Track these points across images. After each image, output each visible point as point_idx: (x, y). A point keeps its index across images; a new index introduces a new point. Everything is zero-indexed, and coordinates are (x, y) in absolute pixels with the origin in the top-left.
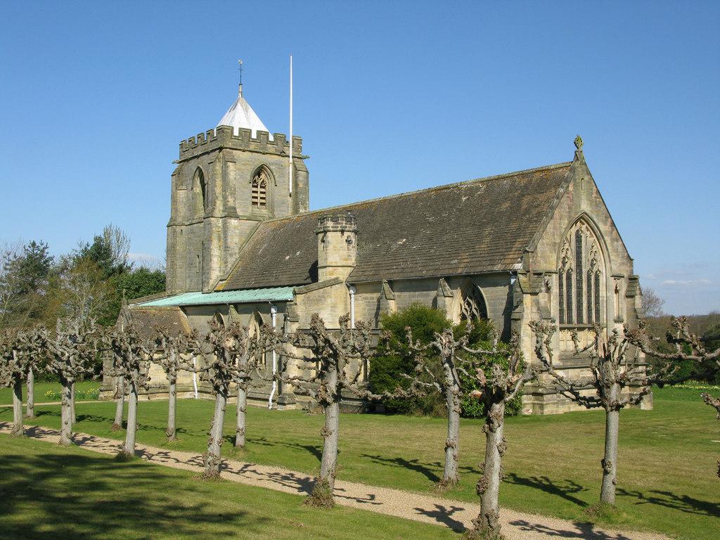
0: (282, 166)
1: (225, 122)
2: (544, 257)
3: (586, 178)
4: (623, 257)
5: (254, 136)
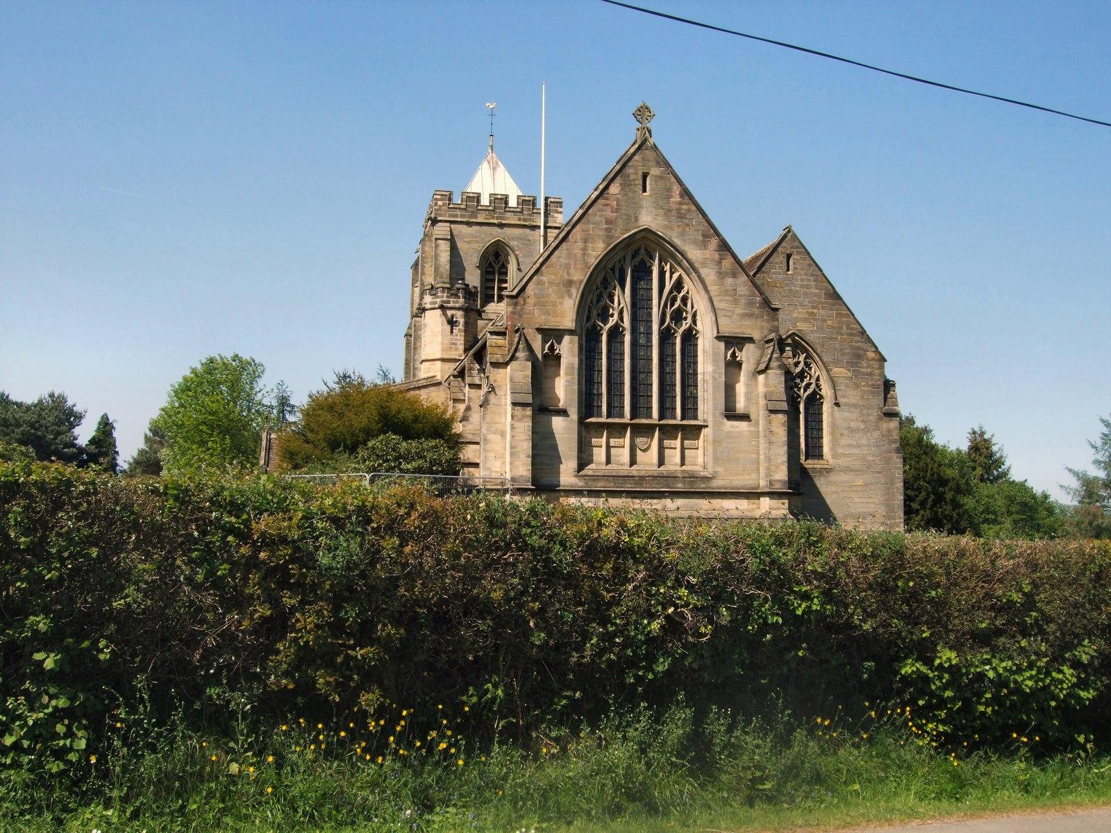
0: (529, 240)
1: (474, 188)
2: (540, 304)
3: (655, 171)
4: (750, 304)
5: (485, 201)
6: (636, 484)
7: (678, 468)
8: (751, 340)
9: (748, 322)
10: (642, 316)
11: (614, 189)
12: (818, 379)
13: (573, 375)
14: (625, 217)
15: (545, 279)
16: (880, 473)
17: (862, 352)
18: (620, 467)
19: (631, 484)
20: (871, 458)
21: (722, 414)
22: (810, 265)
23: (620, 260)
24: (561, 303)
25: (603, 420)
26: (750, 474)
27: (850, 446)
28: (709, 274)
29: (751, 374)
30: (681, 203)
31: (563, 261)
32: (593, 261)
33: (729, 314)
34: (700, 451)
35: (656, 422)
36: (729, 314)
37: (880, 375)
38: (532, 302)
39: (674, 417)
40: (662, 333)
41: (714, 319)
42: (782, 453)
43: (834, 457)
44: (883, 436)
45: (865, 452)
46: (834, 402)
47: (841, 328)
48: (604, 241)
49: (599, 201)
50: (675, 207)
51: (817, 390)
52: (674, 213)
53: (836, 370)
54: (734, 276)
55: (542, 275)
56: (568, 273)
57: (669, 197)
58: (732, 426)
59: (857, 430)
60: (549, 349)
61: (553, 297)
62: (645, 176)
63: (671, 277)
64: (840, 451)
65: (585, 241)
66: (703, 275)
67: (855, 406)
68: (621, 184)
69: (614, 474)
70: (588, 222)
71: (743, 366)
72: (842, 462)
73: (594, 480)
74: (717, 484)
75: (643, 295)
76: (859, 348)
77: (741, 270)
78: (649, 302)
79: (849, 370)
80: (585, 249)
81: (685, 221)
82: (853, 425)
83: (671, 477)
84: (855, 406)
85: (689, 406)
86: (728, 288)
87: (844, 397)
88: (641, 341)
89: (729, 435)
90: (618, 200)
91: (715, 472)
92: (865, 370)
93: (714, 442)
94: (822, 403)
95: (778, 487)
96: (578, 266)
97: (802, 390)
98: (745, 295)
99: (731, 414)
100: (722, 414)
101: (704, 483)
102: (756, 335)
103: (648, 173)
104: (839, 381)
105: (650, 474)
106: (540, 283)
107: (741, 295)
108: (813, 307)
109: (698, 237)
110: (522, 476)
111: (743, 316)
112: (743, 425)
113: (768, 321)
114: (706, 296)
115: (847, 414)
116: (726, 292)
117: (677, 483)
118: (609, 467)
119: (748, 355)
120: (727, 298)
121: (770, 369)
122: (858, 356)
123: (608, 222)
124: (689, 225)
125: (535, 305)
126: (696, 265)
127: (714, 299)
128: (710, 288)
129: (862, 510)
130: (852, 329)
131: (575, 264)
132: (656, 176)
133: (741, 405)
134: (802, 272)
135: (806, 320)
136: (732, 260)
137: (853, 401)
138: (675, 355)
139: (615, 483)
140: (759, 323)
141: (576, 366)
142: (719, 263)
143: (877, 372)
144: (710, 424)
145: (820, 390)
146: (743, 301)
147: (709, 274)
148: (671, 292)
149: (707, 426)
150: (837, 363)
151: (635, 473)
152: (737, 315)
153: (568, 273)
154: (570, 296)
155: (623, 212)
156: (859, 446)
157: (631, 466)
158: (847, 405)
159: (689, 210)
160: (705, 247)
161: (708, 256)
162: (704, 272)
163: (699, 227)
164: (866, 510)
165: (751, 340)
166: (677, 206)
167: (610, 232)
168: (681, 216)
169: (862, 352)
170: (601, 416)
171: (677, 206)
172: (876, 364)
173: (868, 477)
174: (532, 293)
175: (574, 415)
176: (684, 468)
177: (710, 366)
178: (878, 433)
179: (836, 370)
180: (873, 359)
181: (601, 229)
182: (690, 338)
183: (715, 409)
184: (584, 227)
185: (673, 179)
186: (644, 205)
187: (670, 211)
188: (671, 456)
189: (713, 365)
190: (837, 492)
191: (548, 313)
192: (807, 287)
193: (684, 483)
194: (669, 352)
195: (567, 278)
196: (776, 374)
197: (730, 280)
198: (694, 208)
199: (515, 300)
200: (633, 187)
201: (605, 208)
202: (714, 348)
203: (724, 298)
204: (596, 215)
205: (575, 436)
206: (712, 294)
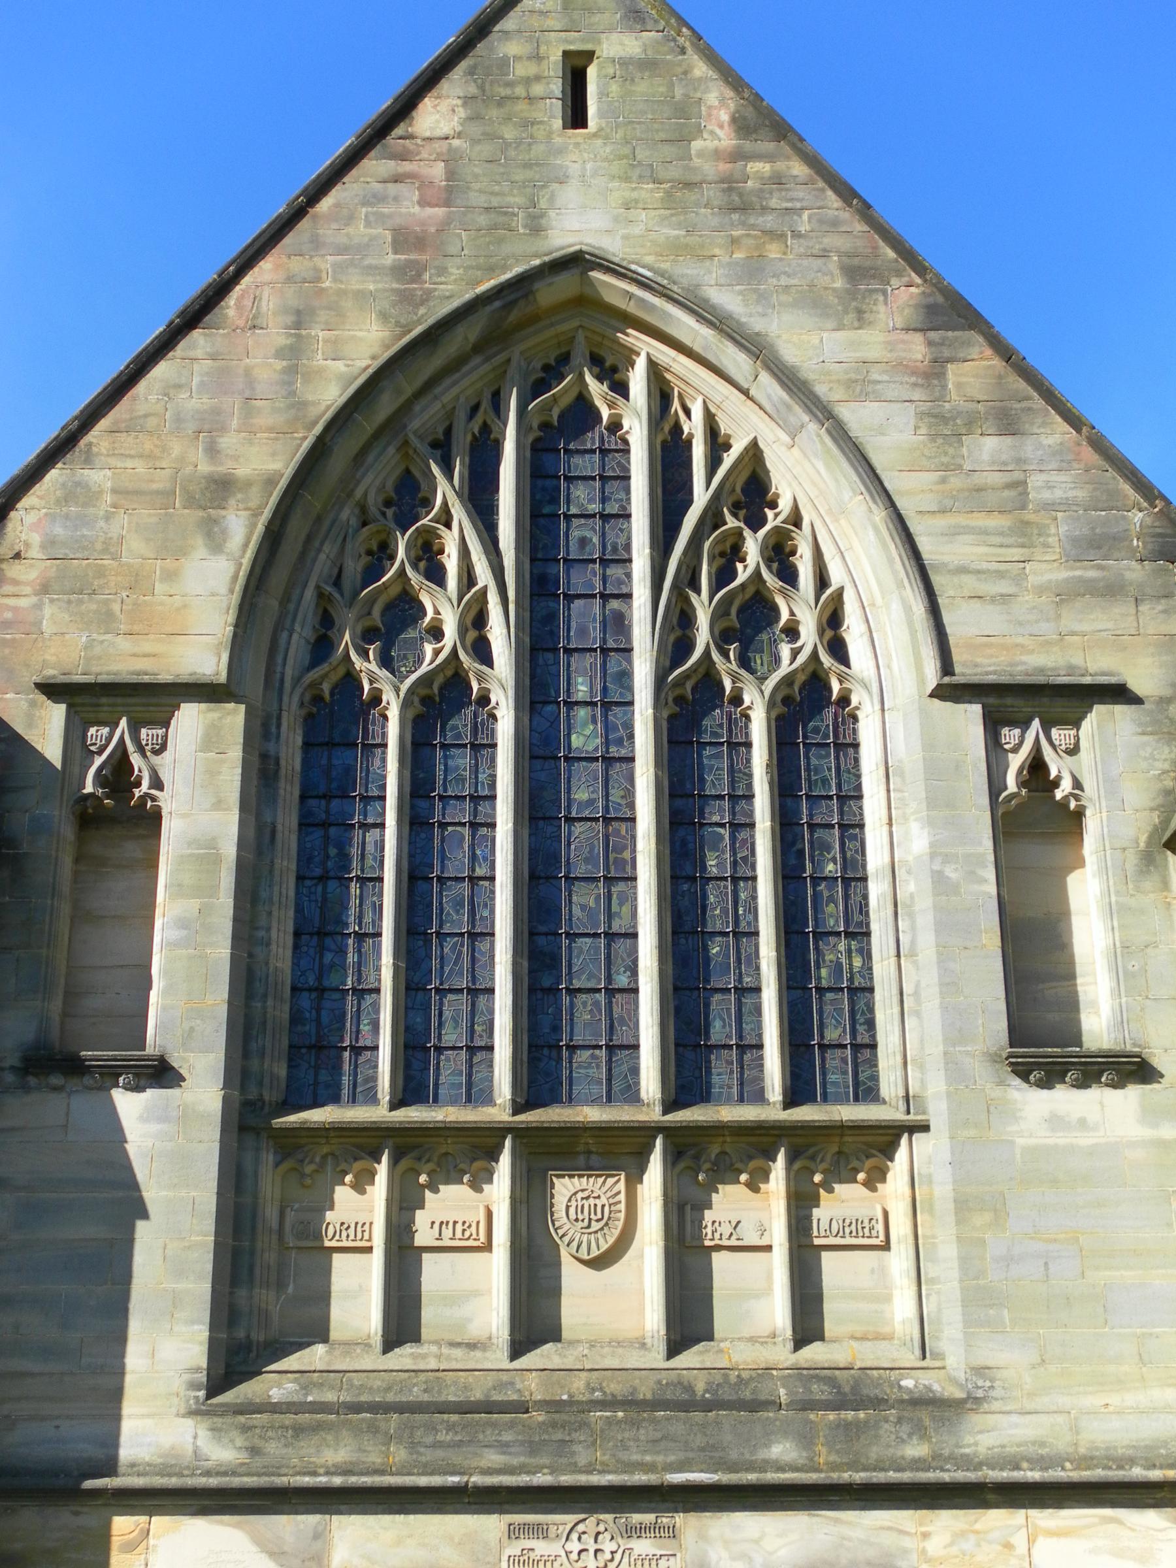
6: (533, 1448)
7: (782, 1354)
8: (1118, 693)
10: (583, 632)
13: (213, 891)
14: (483, 220)
15: (98, 477)
18: (459, 1358)
19: (503, 1447)
21: (994, 1058)
23: (475, 409)
24: (171, 576)
25: (379, 1113)
29: (1132, 860)
30: (737, 156)
31: (193, 403)
33: (1004, 587)
34: (899, 1261)
35: (654, 1114)
36: (1004, 587)
38: (33, 575)
39: (753, 1093)
40: (680, 700)
41: (919, 608)
46: (932, 677)
48: (384, 316)
49: (365, 163)
50: (711, 169)
52: (712, 193)
55: (88, 461)
56: (212, 451)
57: (682, 139)
58: (1056, 1121)
60: (99, 779)
61: (136, 548)
63: (713, 463)
65: (300, 319)
66: (855, 429)
68: (467, 100)
69: (416, 1394)
70: (317, 243)
71: (1092, 824)
73: (299, 1431)
75: (583, 542)
77: (1039, 402)
78: (614, 571)
85: (831, 1035)
86: (978, 479)
88: (576, 741)
90: (451, 160)
91: (980, 1371)
93: (963, 1206)
96: (262, 421)
98: (1066, 505)
100: (994, 1058)
101: (920, 1431)
103: (589, 56)
105: (615, 1387)
106: (73, 494)
107: (1049, 507)
109: (824, 281)
111: (1066, 594)
114: (880, 515)
117: (768, 1439)
118: (403, 1357)
120: (981, 521)
123: (404, 239)
124: (775, 236)
125: (44, 589)
126: (821, 390)
131: (248, 412)
132: (624, 62)
136: (997, 363)
138: (750, 797)
139: (413, 1446)
141: (229, 850)
144: (937, 1112)
146: (1061, 529)
148: (711, 518)
149: (925, 1128)
151: (533, 1388)
152: (1040, 590)
153: (212, 451)
154: (216, 545)
155: (477, 199)
157: (674, 1348)
159: (778, 180)
160: (862, 319)
161: (874, 353)
163: (830, 241)
165: (1118, 693)
166: (724, 167)
167: (417, 278)
170: (373, 1100)
171: (724, 167)
174: (36, 539)
176: (813, 1353)
177: (915, 827)
181: (372, 270)
183: (956, 1035)
184: (297, 265)
185: (701, 69)
186: (574, 169)
187: (688, 185)
188: (452, 1299)
189: (930, 822)
191: (106, 620)
193: (806, 1439)
194: (717, 782)
195: (204, 468)
198: (799, 169)
200: (522, 106)
201: (392, 188)
202: (929, 745)
203: (962, 520)
204: (351, 218)
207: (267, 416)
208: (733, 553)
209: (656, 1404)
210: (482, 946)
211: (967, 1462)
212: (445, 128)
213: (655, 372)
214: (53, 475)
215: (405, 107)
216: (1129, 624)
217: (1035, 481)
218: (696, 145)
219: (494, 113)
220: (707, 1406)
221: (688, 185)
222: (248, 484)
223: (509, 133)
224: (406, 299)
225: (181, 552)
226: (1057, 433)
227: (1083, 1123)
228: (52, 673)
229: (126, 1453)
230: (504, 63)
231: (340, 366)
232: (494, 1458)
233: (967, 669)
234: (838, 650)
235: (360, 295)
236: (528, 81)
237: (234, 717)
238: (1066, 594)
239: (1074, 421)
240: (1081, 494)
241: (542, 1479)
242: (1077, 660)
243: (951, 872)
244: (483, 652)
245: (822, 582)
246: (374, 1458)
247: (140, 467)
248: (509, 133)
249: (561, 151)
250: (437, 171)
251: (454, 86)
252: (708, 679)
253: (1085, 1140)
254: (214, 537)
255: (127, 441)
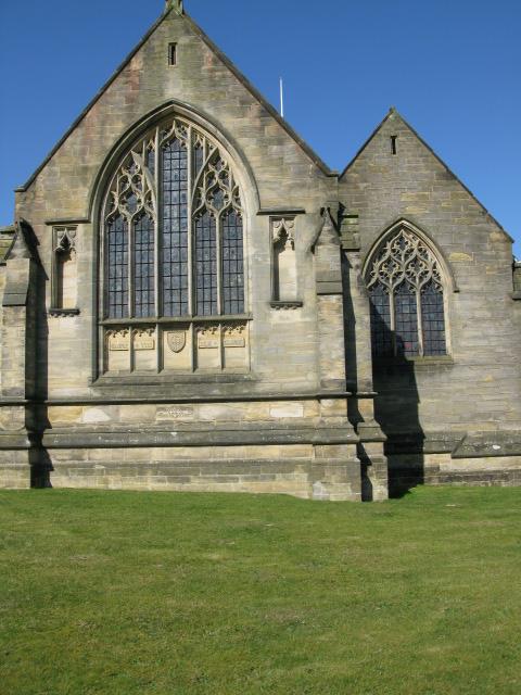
2: (52, 196)
4: (301, 173)
9: (297, 194)
11: (136, 64)
12: (435, 267)
13: (87, 270)
15: (57, 169)
16: (513, 366)
17: (484, 233)
20: (501, 350)
22: (418, 146)
26: (306, 375)
27: (475, 337)
28: (249, 145)
30: (212, 71)
32: (110, 143)
34: (246, 350)
37: (506, 257)
42: (337, 346)
43: (455, 351)
44: (515, 324)
45: (493, 344)
47: (458, 210)
48: (123, 121)
51: (435, 278)
53: (454, 255)
54: (280, 142)
55: (54, 165)
56: (83, 161)
58: (281, 318)
59: (483, 320)
62: (173, 46)
63: (207, 154)
64: (463, 343)
67: (479, 293)
68: (144, 59)
72: (467, 356)
74: (262, 388)
76: (480, 230)
79: (470, 255)
80: (102, 132)
81: (221, 89)
82: (478, 314)
83: (207, 381)
84: (479, 293)
87: (465, 283)
89: (278, 329)
92: (489, 253)
94: (441, 292)
95: (332, 389)
97: (417, 280)
99: (277, 302)
102: (310, 208)
104: (459, 266)
105: (180, 380)
106: (52, 174)
108: (424, 190)
110: (14, 389)
112: (294, 316)
113: (324, 190)
115: (469, 303)
116: (271, 162)
119: (301, 231)
121: (321, 244)
122: (480, 238)
124: (222, 92)
127: (255, 171)
128: (250, 158)
129: (491, 409)
130: (471, 209)
133: (288, 291)
134: (410, 154)
135: (416, 203)
137: (476, 287)
140: (313, 193)
141: (91, 260)
142: (262, 128)
143: (503, 254)
145: (439, 278)
147: (249, 145)
148: (206, 168)
150: (455, 246)
151: (162, 380)
153: (83, 161)
156: (485, 337)
158: (470, 292)
159: (224, 77)
162: (242, 141)
164: (497, 408)
165: (303, 212)
168: (214, 84)
169: (484, 233)
170: (127, 317)
172: (502, 246)
173: (498, 372)
175: (87, 315)
178: (508, 321)
179: (454, 255)
180: (498, 240)
181: (121, 109)
182: (231, 217)
184: (102, 108)
185: (205, 46)
190: (461, 391)
191: (60, 206)
192: (416, 168)
193: (221, 389)
196: (329, 249)
197: (275, 147)
198: (229, 73)
199: (25, 194)
205: (89, 339)
206: (253, 165)
207: (96, 148)
208: (211, 176)
209: (189, 382)
210: (151, 279)
211: (255, 394)
212: (138, 68)
213: (194, 131)
214: (46, 168)
215: (128, 62)
216: (306, 195)
217: (286, 157)
218: (203, 68)
219: (151, 63)
220: (199, 383)
221: (201, 80)
222: (91, 168)
223: (155, 68)
224: (130, 116)
225: (77, 187)
226: (291, 144)
227: (288, 318)
228: (49, 220)
229: (49, 396)
230: (153, 48)
231: (113, 135)
232: (154, 395)
233: (264, 208)
234: (237, 200)
235: (118, 115)
236: (160, 53)
237: (90, 228)
238: (291, 187)
239: (296, 140)
240: (297, 160)
241: (164, 399)
242: (294, 205)
243: (260, 259)
244: (150, 204)
245: (234, 184)
246: (128, 395)
247: (66, 166)
248: (155, 68)
249: (168, 72)
250: (137, 80)
251: (140, 55)
252: (204, 210)
253: (287, 322)
254: (85, 182)
255: (64, 159)
